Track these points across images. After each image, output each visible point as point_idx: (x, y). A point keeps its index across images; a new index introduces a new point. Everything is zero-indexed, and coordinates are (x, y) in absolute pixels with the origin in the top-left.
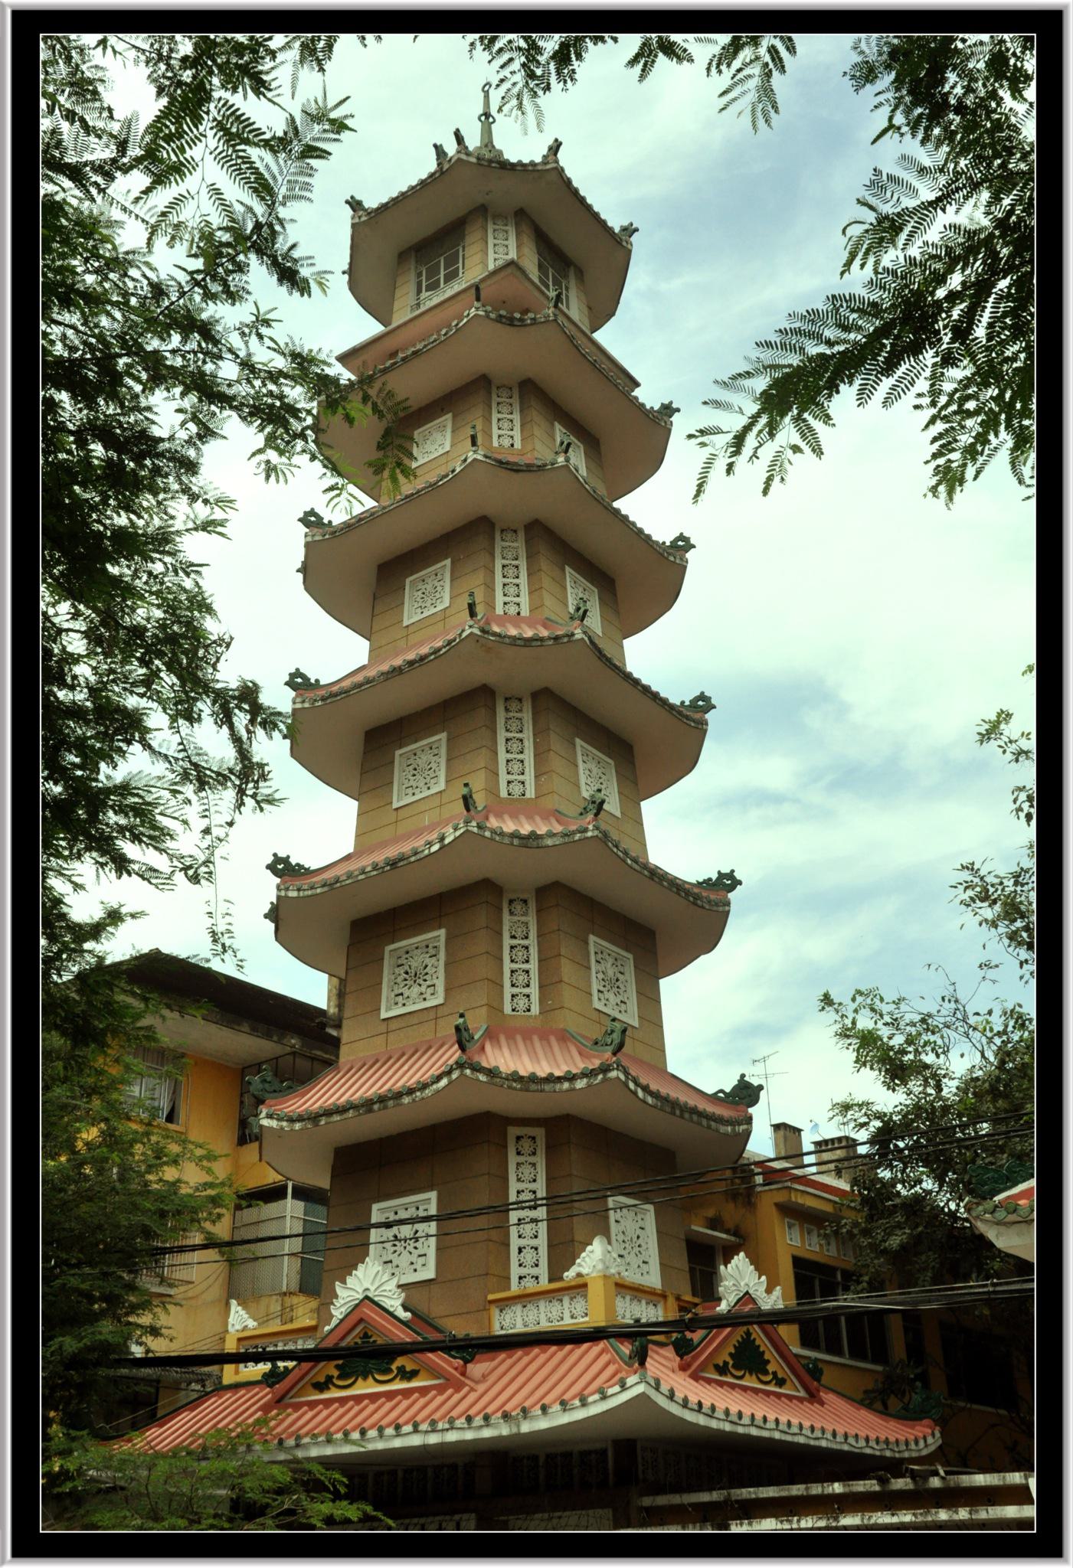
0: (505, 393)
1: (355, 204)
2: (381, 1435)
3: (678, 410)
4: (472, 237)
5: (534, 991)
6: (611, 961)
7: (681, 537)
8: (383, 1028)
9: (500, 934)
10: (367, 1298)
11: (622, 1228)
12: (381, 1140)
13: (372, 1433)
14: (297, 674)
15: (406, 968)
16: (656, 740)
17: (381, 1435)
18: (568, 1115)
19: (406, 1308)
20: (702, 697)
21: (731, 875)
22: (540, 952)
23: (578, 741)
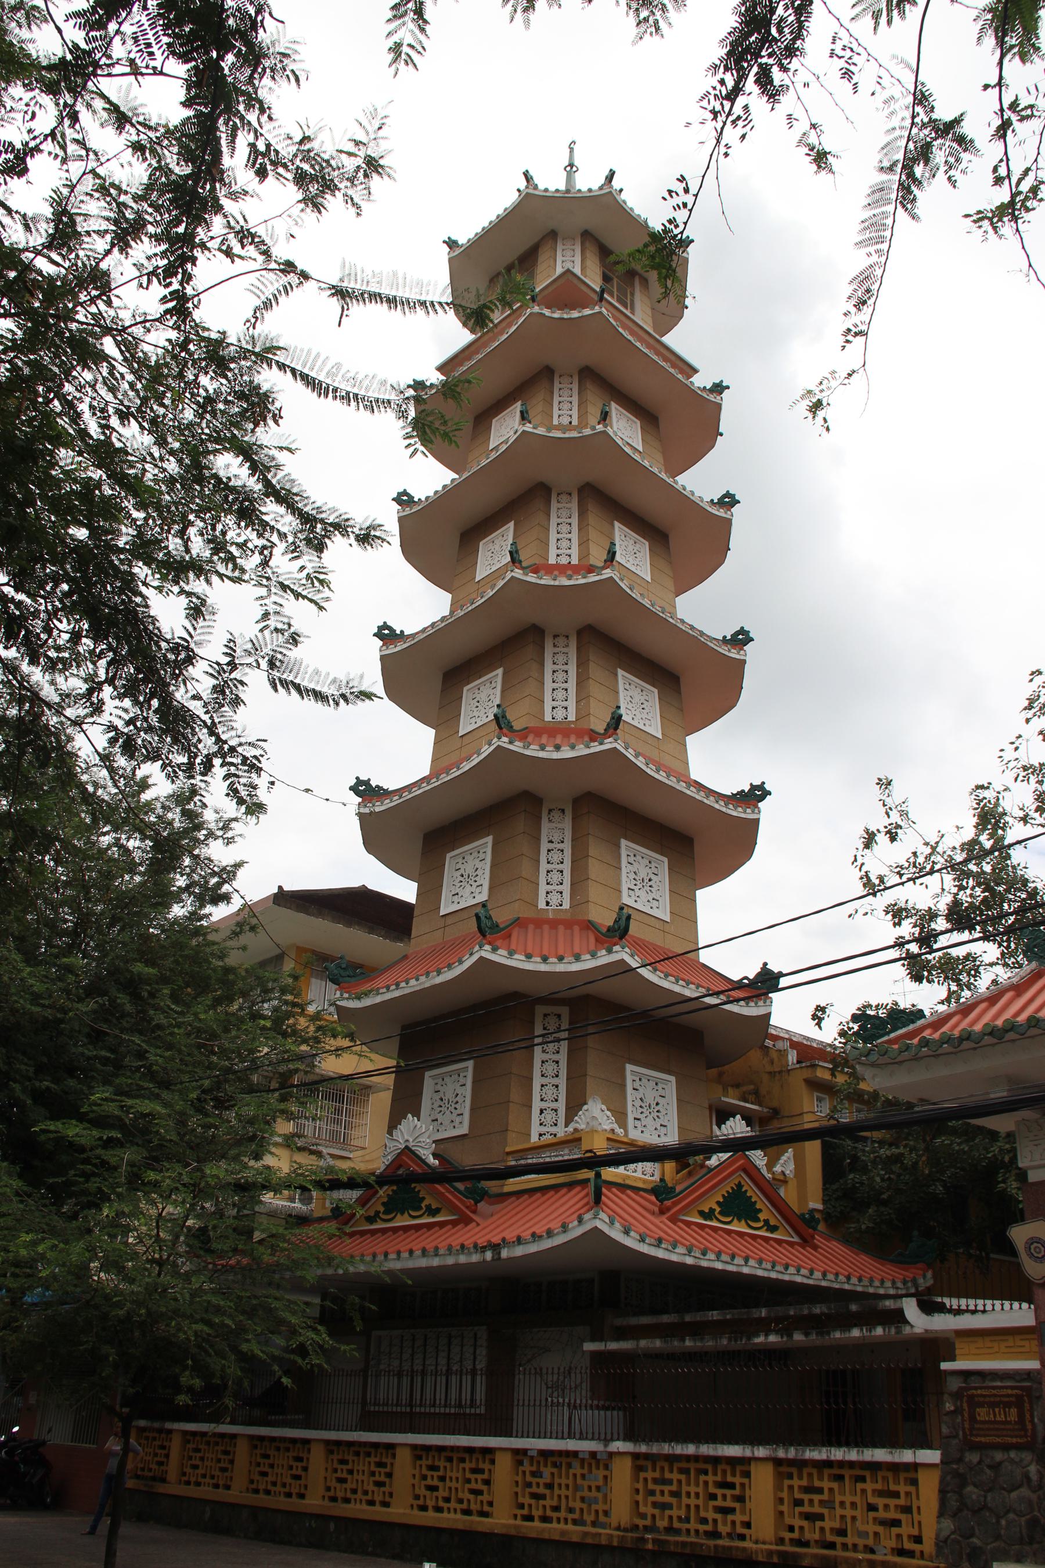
0: (564, 497)
1: (451, 244)
2: (399, 1257)
3: (728, 387)
4: (543, 257)
5: (566, 888)
6: (646, 861)
7: (742, 631)
9: (539, 839)
10: (407, 1147)
11: (639, 1095)
13: (392, 1256)
14: (385, 626)
15: (462, 871)
16: (701, 680)
17: (399, 1257)
19: (435, 1156)
20: (742, 631)
21: (761, 787)
22: (573, 854)
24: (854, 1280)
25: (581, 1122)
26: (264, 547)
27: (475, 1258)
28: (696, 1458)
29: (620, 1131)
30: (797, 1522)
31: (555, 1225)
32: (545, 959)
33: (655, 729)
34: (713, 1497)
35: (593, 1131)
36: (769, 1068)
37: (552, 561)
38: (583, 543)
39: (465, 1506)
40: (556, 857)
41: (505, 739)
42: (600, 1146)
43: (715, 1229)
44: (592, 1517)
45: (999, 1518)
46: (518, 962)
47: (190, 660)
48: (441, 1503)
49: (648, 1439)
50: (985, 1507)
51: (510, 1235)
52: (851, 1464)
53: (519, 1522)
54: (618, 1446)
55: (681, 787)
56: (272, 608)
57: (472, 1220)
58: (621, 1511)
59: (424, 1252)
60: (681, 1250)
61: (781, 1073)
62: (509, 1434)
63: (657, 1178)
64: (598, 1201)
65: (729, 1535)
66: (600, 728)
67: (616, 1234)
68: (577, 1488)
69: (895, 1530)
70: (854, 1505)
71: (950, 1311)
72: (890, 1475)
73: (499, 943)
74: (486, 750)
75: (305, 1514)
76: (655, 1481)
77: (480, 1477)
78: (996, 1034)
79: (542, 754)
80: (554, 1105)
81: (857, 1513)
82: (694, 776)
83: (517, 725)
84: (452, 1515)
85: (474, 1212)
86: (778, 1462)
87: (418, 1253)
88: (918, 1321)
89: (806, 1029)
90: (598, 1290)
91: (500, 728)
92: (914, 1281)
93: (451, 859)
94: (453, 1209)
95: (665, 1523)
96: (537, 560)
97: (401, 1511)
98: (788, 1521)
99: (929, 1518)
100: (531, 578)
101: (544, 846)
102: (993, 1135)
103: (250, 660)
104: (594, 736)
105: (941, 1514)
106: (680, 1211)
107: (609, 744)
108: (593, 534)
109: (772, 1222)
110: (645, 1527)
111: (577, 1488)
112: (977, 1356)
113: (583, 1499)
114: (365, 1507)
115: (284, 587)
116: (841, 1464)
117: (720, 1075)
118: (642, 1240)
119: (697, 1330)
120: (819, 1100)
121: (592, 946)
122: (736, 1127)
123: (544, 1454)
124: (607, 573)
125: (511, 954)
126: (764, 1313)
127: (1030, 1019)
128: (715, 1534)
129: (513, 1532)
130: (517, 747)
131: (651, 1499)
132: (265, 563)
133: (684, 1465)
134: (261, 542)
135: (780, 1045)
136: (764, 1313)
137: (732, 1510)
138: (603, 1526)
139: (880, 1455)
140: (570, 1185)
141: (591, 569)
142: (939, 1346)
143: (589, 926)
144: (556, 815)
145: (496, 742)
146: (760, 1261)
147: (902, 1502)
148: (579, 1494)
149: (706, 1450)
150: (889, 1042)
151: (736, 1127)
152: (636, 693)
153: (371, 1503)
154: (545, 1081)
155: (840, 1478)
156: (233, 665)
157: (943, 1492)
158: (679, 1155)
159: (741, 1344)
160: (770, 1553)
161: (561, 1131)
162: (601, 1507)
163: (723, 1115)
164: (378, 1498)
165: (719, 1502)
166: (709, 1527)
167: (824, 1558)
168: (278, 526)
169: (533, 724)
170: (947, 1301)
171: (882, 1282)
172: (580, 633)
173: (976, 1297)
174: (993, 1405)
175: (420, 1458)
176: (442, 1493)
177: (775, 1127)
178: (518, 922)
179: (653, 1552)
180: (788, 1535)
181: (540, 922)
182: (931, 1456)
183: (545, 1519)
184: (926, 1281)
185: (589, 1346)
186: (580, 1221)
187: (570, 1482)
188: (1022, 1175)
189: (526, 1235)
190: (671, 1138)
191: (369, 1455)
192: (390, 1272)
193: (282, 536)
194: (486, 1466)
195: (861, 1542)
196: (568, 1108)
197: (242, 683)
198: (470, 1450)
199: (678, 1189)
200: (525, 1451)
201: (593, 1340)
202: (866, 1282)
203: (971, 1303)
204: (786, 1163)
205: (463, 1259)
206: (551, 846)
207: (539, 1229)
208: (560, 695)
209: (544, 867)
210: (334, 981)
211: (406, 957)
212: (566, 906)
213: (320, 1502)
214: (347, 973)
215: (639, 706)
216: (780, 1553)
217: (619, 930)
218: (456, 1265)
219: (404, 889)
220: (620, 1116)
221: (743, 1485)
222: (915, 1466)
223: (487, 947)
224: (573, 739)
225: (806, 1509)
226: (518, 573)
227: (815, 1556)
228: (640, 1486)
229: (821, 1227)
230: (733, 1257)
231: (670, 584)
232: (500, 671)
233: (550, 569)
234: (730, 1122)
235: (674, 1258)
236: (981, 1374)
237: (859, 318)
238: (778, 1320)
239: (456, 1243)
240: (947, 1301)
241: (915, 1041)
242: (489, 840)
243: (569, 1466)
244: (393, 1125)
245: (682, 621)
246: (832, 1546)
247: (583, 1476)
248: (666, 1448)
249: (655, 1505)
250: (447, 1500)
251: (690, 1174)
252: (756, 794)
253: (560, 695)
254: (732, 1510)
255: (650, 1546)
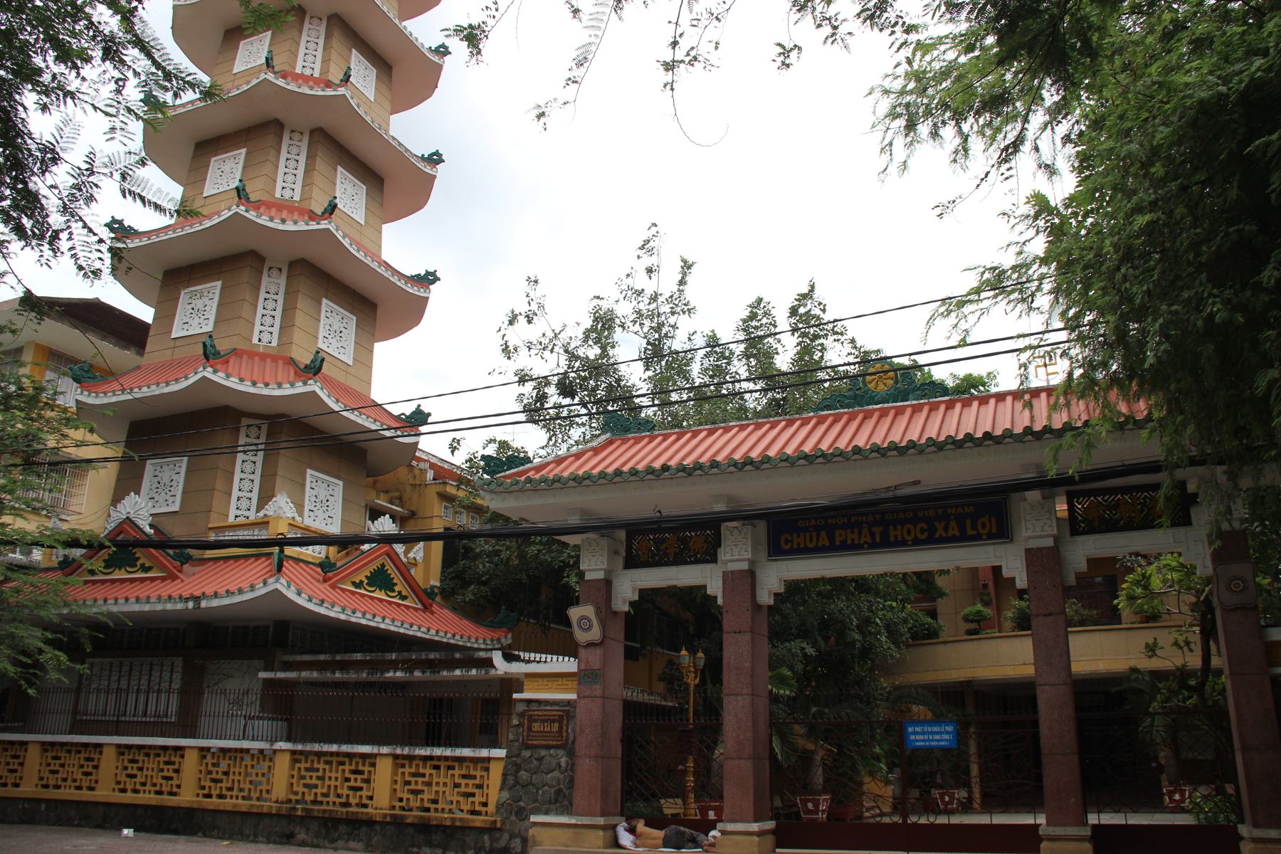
0: (315, 21)
2: (116, 603)
5: (276, 330)
7: (437, 153)
8: (172, 344)
11: (315, 493)
12: (159, 418)
16: (398, 183)
17: (116, 603)
18: (227, 407)
19: (151, 526)
20: (437, 153)
21: (433, 274)
23: (339, 168)
24: (458, 637)
25: (270, 510)
26: (120, 79)
27: (180, 606)
28: (338, 754)
29: (298, 519)
30: (405, 796)
31: (246, 585)
32: (254, 384)
33: (360, 216)
34: (348, 780)
35: (279, 518)
36: (412, 481)
37: (298, 70)
38: (326, 61)
39: (157, 788)
40: (271, 305)
41: (242, 208)
42: (282, 529)
43: (363, 595)
44: (257, 795)
45: (538, 789)
46: (233, 383)
47: (56, 160)
48: (138, 787)
49: (304, 740)
50: (531, 783)
51: (209, 590)
52: (446, 758)
53: (201, 799)
54: (281, 745)
55: (375, 265)
56: (118, 125)
57: (178, 578)
58: (279, 789)
59: (138, 600)
60: (337, 609)
61: (420, 486)
62: (193, 736)
63: (323, 555)
64: (280, 568)
65: (357, 805)
66: (319, 211)
67: (291, 594)
68: (247, 774)
69: (471, 799)
70: (445, 784)
71: (523, 661)
72: (471, 765)
73: (219, 367)
74: (226, 214)
75: (20, 799)
76: (307, 769)
77: (171, 767)
78: (578, 480)
79: (270, 224)
80: (249, 495)
81: (447, 789)
82: (384, 257)
83: (253, 197)
84: (147, 795)
85: (180, 571)
86: (396, 757)
87: (133, 600)
88: (501, 666)
89: (445, 454)
90: (271, 635)
91: (240, 198)
92: (499, 640)
93: (184, 295)
94: (163, 568)
95: (312, 798)
96: (287, 68)
97: (105, 793)
98: (399, 795)
99: (494, 791)
100: (281, 82)
101: (262, 295)
102: (565, 545)
103: (107, 171)
104: (312, 216)
105: (501, 789)
106: (338, 581)
107: (324, 225)
108: (334, 56)
109: (404, 593)
110: (297, 801)
111: (247, 774)
112: (538, 690)
113: (251, 782)
114: (73, 791)
115: (129, 110)
116: (439, 758)
117: (375, 482)
118: (310, 600)
119: (344, 666)
120: (446, 508)
121: (292, 379)
122: (385, 525)
123: (224, 751)
124: (341, 91)
125: (228, 376)
126: (394, 656)
127: (600, 473)
128: (347, 804)
129: (196, 806)
130: (252, 215)
131: (302, 781)
132: (118, 92)
133: (328, 758)
134: (117, 74)
135: (422, 465)
136: (394, 656)
137: (361, 789)
138: (266, 800)
139: (466, 752)
140: (258, 556)
141: (329, 84)
142: (512, 684)
143: (291, 362)
144: (275, 272)
145: (234, 209)
146: (393, 620)
147: (477, 782)
148: (248, 779)
149: (345, 748)
150: (505, 477)
151: (385, 525)
152: (349, 187)
153: (79, 788)
154: (243, 476)
155: (437, 767)
156: (92, 172)
157: (505, 775)
158: (344, 543)
159: (377, 677)
160: (385, 816)
161: (252, 516)
162: (264, 787)
163: (375, 514)
164: (85, 784)
165: (352, 783)
166: (343, 800)
167: (422, 817)
168: (135, 67)
169: (265, 197)
170: (522, 654)
171: (477, 639)
172: (312, 132)
173: (530, 652)
174: (543, 721)
175: (123, 754)
176: (139, 780)
177: (412, 528)
178: (235, 352)
179: (302, 817)
180: (398, 804)
181: (252, 354)
182: (500, 753)
183: (221, 796)
184: (508, 640)
185: (262, 675)
186: (265, 583)
187: (242, 770)
188: (581, 575)
189: (222, 591)
190: (334, 528)
191: (79, 752)
192: (111, 615)
193: (136, 74)
194: (177, 760)
195: (447, 807)
196: (259, 499)
197: (97, 186)
198: (165, 748)
199: (339, 564)
200: (208, 749)
201: (266, 670)
202: (465, 639)
203: (538, 656)
204: (418, 551)
205: (169, 606)
206: (267, 296)
207: (233, 588)
208: (290, 178)
209: (260, 311)
210: (76, 380)
211: (139, 368)
212: (274, 343)
213: (34, 789)
214: (87, 374)
215: (350, 196)
216: (392, 816)
217: (314, 369)
218: (164, 611)
219: (145, 313)
220: (300, 507)
221: (370, 772)
222: (489, 759)
223: (210, 369)
224: (296, 216)
225: (413, 787)
226: (270, 76)
227: (416, 817)
228: (295, 773)
229: (438, 599)
230: (374, 616)
231: (388, 106)
232: (244, 151)
233: (297, 77)
234: (381, 519)
235: (332, 614)
236: (538, 702)
237: (578, 73)
238: (405, 662)
239: (165, 594)
240: (522, 654)
241: (523, 479)
242: (219, 284)
243: (242, 759)
244: (116, 499)
245: (394, 139)
246: (428, 810)
247: (253, 766)
248: (317, 747)
249: (305, 785)
250: (144, 784)
251: (347, 554)
252: (429, 279)
253: (290, 178)
254: (361, 789)
255: (299, 813)
